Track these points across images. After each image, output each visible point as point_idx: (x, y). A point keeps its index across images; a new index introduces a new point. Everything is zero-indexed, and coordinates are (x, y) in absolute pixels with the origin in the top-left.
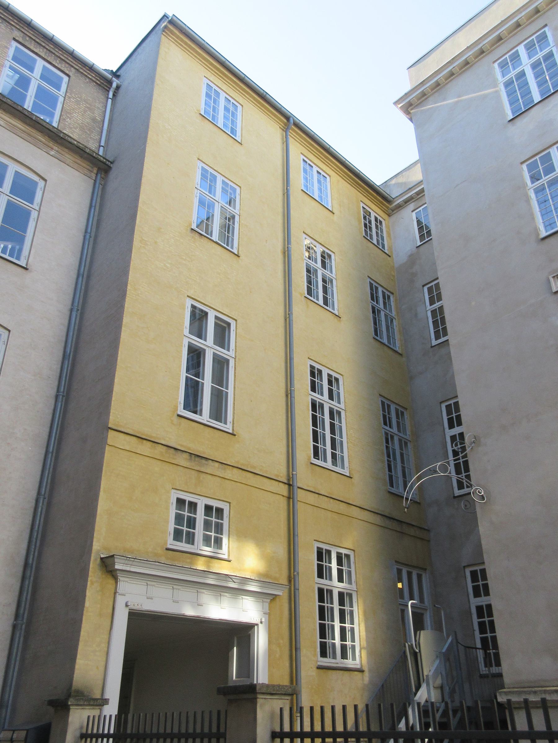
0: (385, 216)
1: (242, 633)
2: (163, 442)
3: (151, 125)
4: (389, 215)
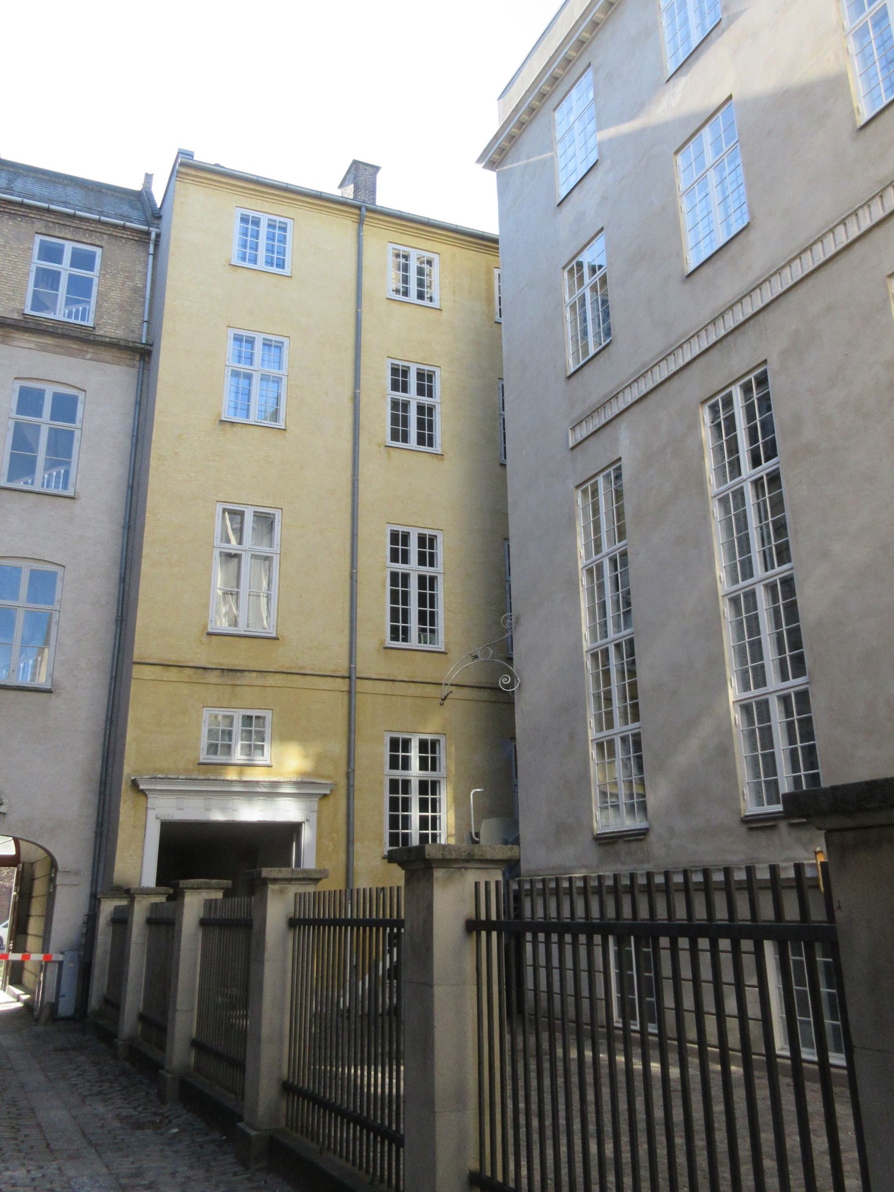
1: (293, 829)
2: (192, 664)
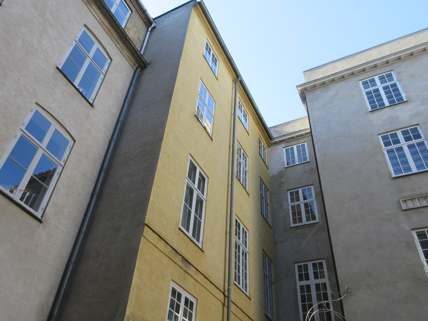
0: (267, 147)
3: (184, 50)
4: (269, 146)
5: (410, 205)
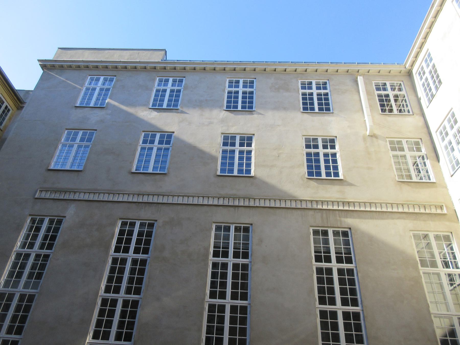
5: (43, 195)
